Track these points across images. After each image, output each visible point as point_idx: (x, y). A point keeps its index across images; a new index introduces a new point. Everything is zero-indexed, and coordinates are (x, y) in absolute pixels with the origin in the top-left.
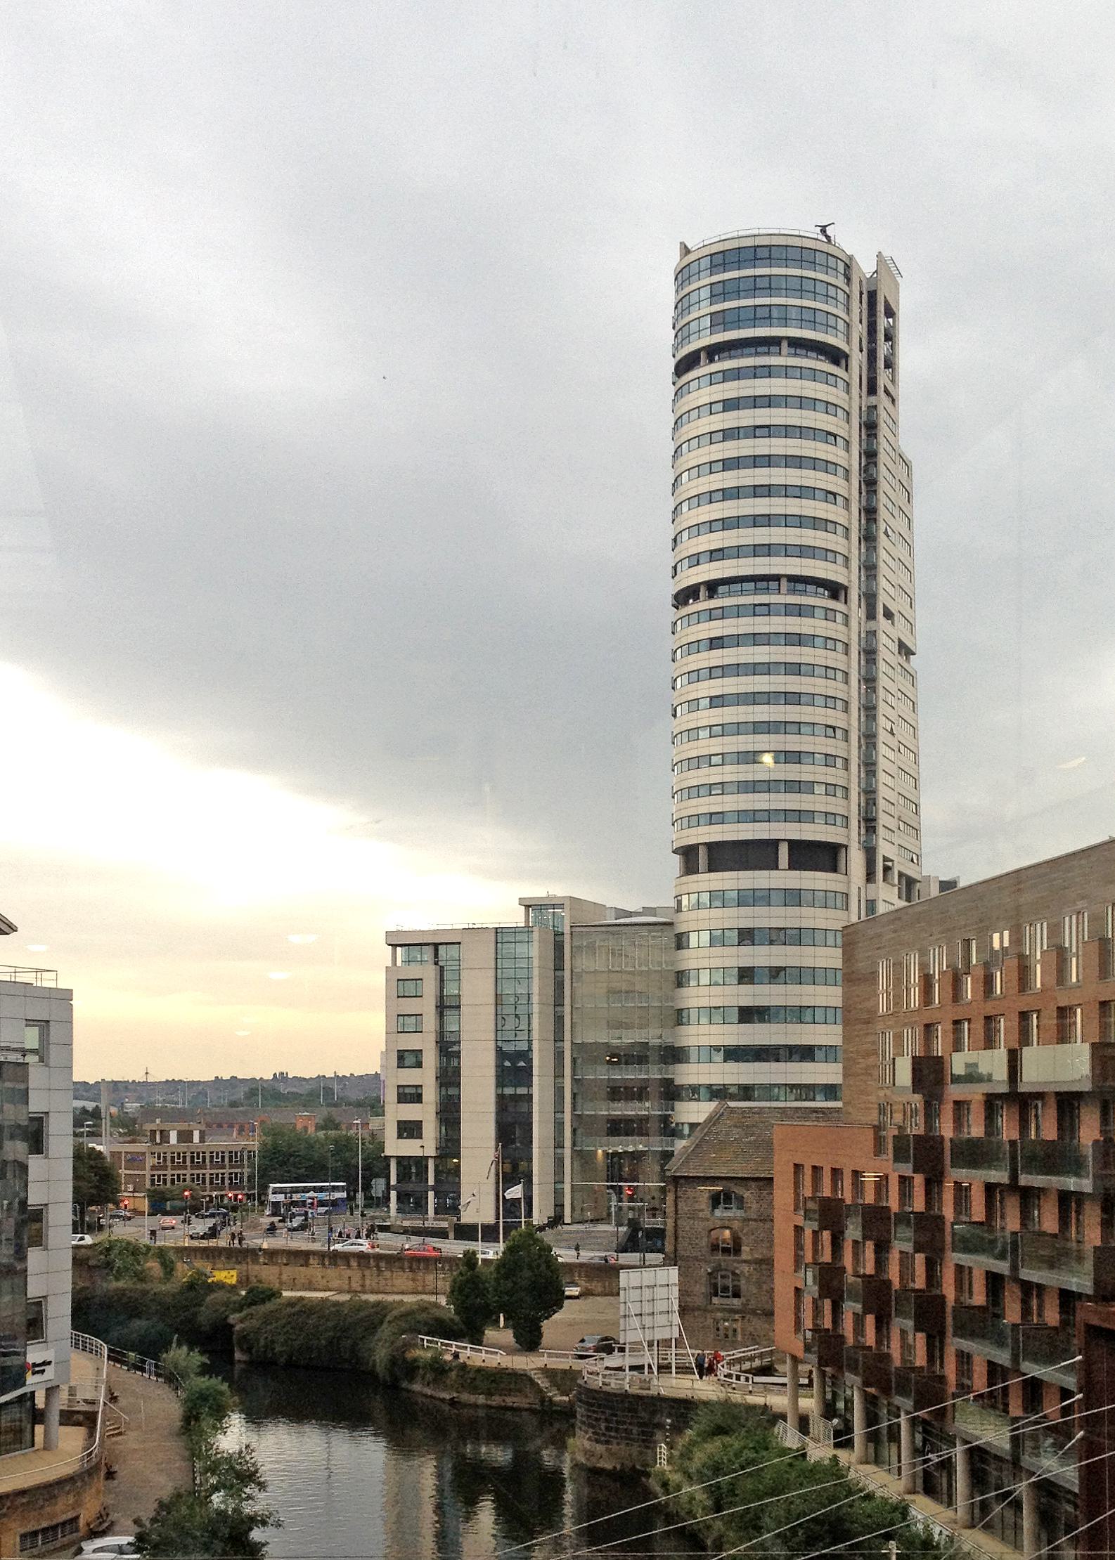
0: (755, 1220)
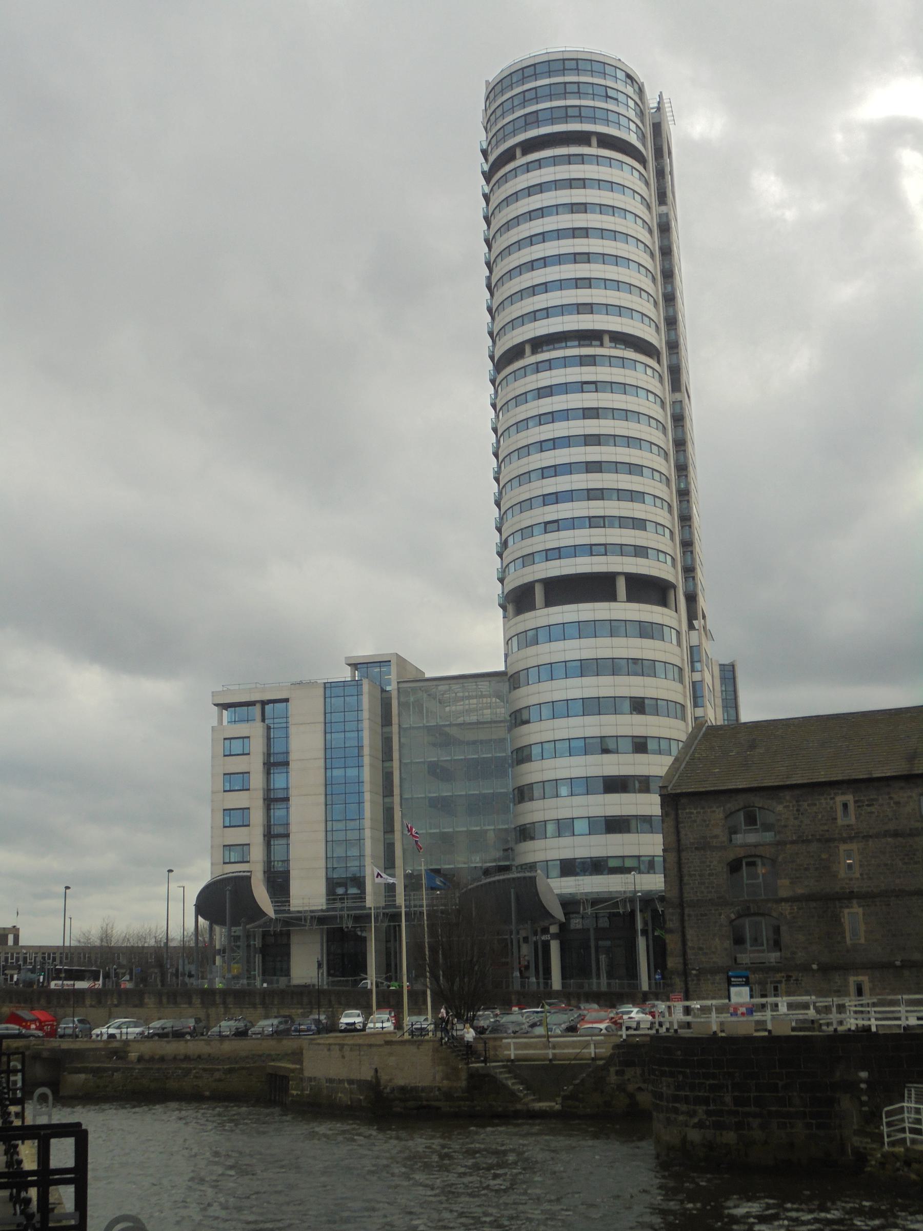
0: (793, 842)
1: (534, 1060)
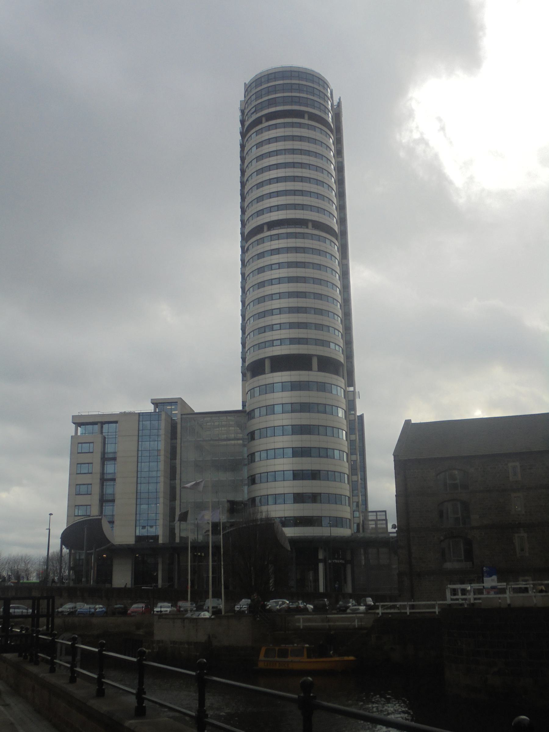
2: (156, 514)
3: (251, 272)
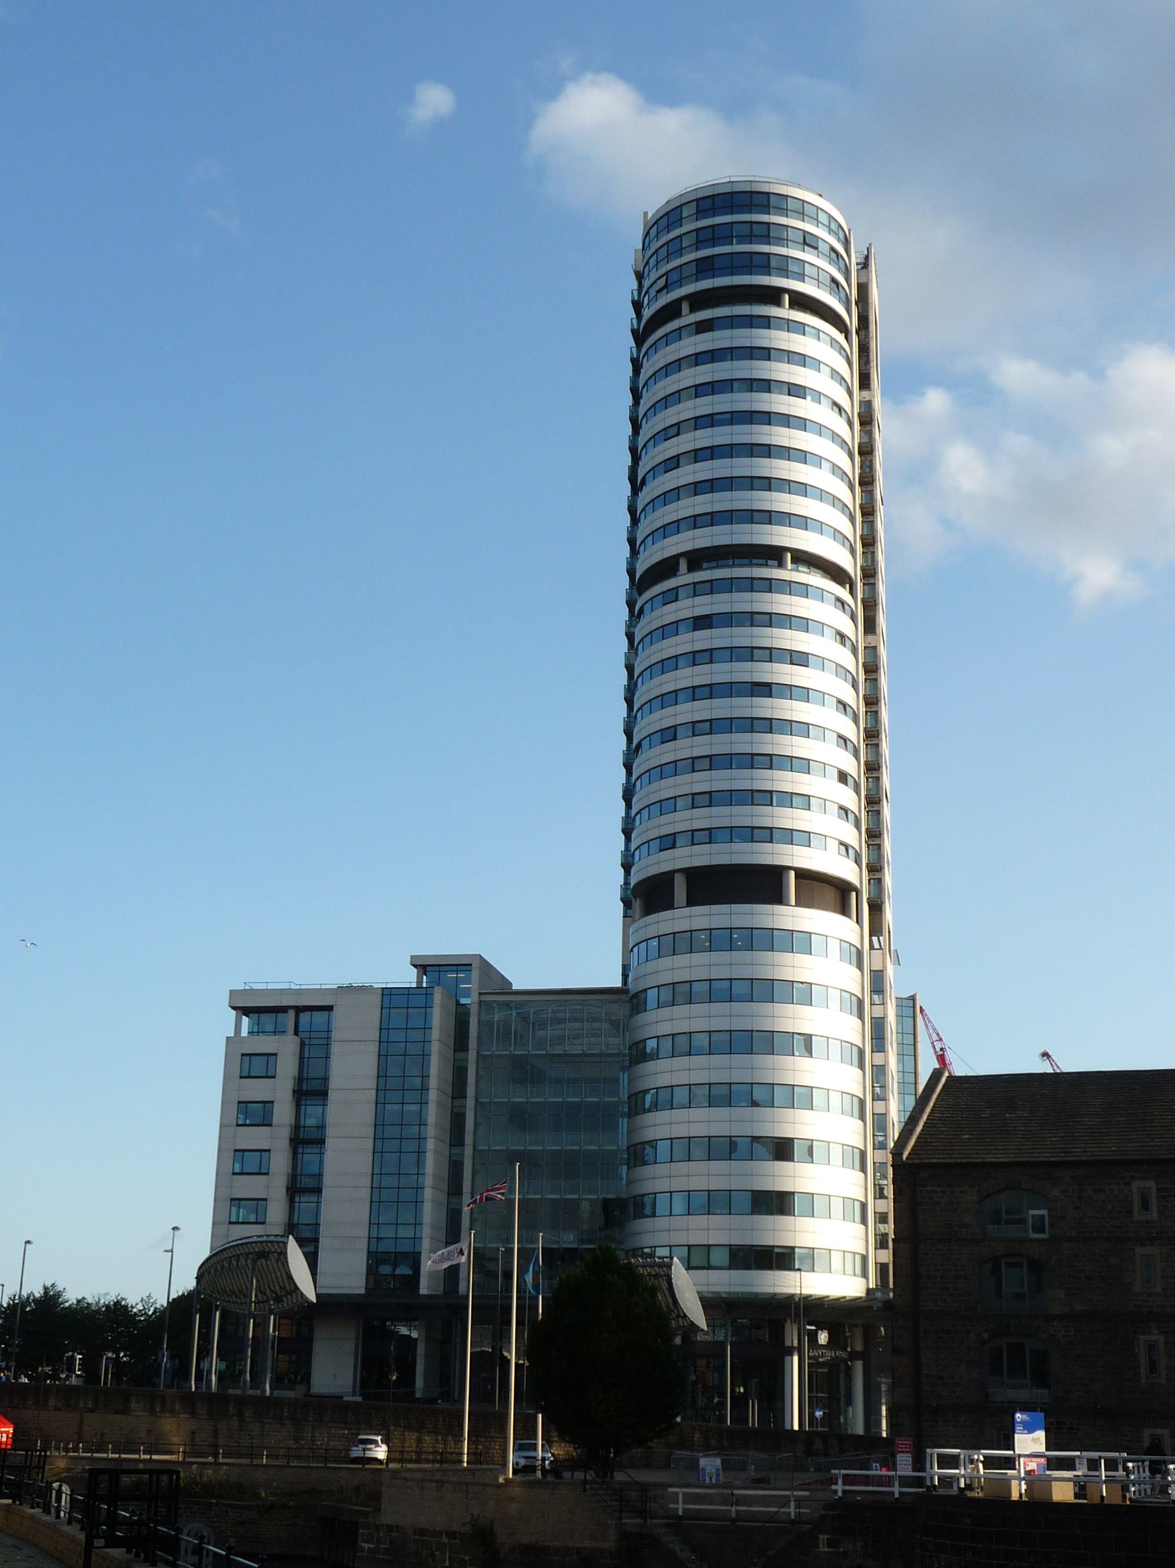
1: (705, 1519)
2: (419, 1152)
3: (648, 668)
